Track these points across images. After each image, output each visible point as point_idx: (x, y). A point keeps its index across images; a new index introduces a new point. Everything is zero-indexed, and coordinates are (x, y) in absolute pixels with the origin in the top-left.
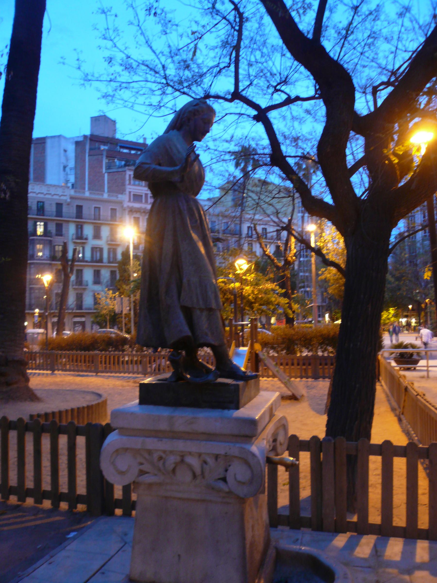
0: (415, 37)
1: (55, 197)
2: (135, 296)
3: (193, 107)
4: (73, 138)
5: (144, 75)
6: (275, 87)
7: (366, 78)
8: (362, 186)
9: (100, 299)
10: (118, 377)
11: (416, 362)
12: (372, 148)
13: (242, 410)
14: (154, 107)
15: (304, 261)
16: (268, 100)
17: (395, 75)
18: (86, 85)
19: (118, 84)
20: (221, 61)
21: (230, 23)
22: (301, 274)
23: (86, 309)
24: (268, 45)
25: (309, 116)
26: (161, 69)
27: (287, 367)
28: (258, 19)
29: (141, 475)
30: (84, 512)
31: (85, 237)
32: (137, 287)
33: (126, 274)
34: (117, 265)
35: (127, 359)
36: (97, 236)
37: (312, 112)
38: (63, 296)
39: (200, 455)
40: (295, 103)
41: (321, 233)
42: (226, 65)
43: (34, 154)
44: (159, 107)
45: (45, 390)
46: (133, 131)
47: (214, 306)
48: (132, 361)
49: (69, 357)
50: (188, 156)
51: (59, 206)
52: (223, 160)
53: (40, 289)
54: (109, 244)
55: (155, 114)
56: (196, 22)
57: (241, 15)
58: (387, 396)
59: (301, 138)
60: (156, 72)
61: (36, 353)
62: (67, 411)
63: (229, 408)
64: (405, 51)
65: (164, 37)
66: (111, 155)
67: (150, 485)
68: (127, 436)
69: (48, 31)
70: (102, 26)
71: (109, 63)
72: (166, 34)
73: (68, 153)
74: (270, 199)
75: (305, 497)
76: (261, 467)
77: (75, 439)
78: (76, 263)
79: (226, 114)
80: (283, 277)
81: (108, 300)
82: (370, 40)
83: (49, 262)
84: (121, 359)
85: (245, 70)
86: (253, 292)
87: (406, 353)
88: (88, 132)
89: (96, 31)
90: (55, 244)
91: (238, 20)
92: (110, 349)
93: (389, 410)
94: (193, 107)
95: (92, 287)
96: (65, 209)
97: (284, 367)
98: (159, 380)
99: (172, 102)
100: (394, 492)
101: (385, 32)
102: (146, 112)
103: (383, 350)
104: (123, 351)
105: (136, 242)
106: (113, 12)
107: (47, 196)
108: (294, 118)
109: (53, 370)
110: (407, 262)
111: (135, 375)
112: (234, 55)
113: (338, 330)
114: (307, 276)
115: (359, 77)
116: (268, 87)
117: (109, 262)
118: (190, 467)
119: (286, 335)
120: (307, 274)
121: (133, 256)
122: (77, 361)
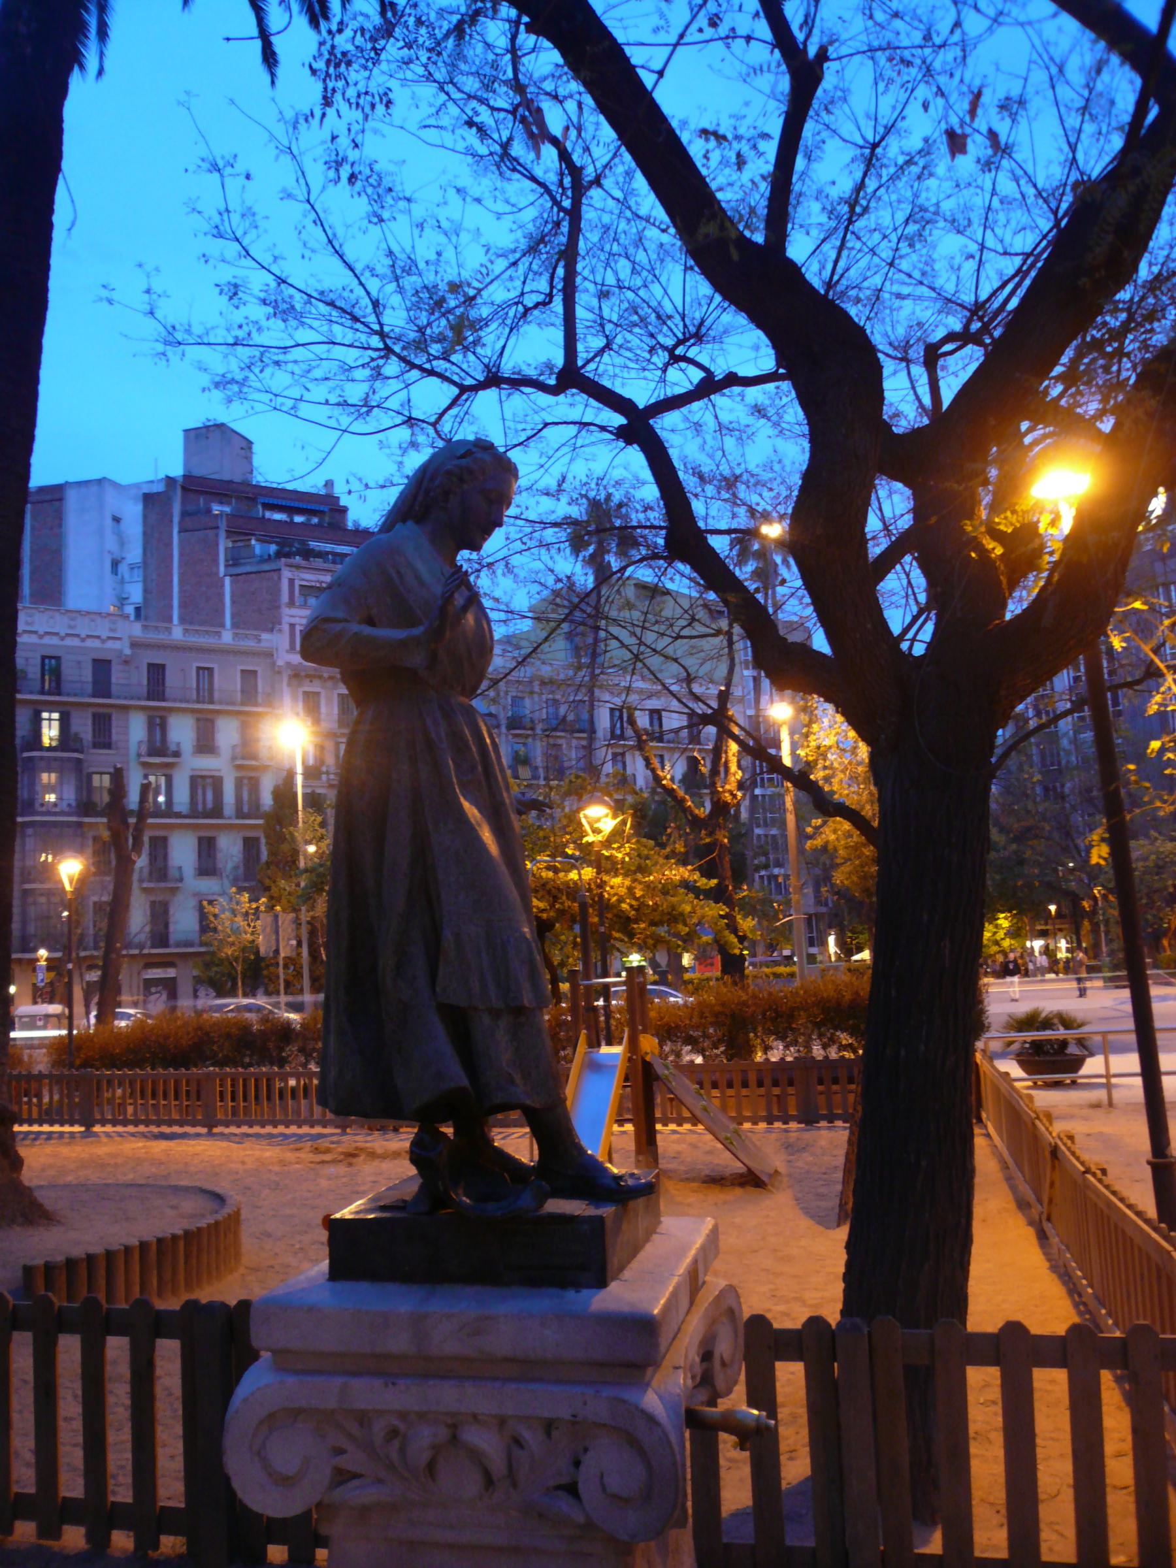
0: (1025, 219)
1: (90, 643)
2: (312, 908)
3: (456, 462)
4: (137, 486)
5: (325, 328)
6: (671, 351)
7: (905, 324)
8: (912, 602)
9: (215, 916)
10: (271, 1136)
11: (1077, 1063)
12: (933, 520)
13: (614, 1286)
14: (352, 409)
15: (763, 796)
16: (653, 385)
17: (980, 319)
18: (169, 354)
19: (256, 352)
20: (527, 289)
21: (548, 191)
22: (758, 831)
23: (178, 945)
24: (647, 244)
25: (763, 421)
26: (370, 309)
27: (730, 1092)
28: (621, 180)
29: (341, 1483)
30: (180, 1557)
31: (173, 747)
32: (316, 887)
33: (285, 847)
34: (261, 822)
35: (292, 1082)
36: (205, 745)
37: (771, 412)
38: (116, 910)
39: (502, 1422)
40: (726, 391)
41: (809, 725)
42: (541, 298)
43: (33, 527)
44: (367, 407)
45: (67, 1186)
46: (297, 475)
47: (527, 1000)
48: (306, 1089)
49: (132, 1083)
50: (448, 598)
51: (102, 667)
52: (541, 545)
53: (50, 893)
54: (239, 767)
55: (358, 427)
56: (458, 191)
57: (575, 171)
58: (1005, 1167)
59: (745, 477)
60: (355, 319)
61: (41, 1076)
62: (128, 1250)
63: (578, 1286)
64: (1005, 253)
65: (375, 231)
66: (240, 529)
67: (364, 1512)
68: (297, 1372)
69: (68, 226)
70: (211, 203)
71: (231, 298)
72: (381, 220)
73: (123, 524)
74: (667, 640)
75: (795, 1482)
76: (673, 1454)
77: (152, 1348)
78: (150, 821)
79: (546, 425)
80: (710, 848)
81: (239, 919)
82: (912, 228)
83: (74, 819)
84: (278, 1084)
85: (591, 310)
86: (630, 890)
87: (1049, 1041)
88: (176, 468)
89: (195, 215)
90: (92, 769)
91: (567, 181)
92: (247, 1060)
93: (1012, 1206)
94: (456, 462)
95: (195, 884)
96: (117, 676)
97: (723, 1093)
98: (383, 1208)
99: (403, 395)
100: (1040, 1453)
101: (947, 206)
102: (334, 424)
103: (988, 1035)
104: (282, 1062)
105: (311, 762)
106: (240, 167)
107: (69, 642)
108: (722, 428)
109: (89, 1123)
110: (1038, 790)
111: (318, 1130)
112: (560, 271)
113: (864, 985)
114: (774, 836)
115: (888, 320)
116: (652, 350)
117: (240, 814)
118: (476, 1456)
119: (723, 1005)
120: (774, 831)
121: (305, 795)
122: (154, 1095)
